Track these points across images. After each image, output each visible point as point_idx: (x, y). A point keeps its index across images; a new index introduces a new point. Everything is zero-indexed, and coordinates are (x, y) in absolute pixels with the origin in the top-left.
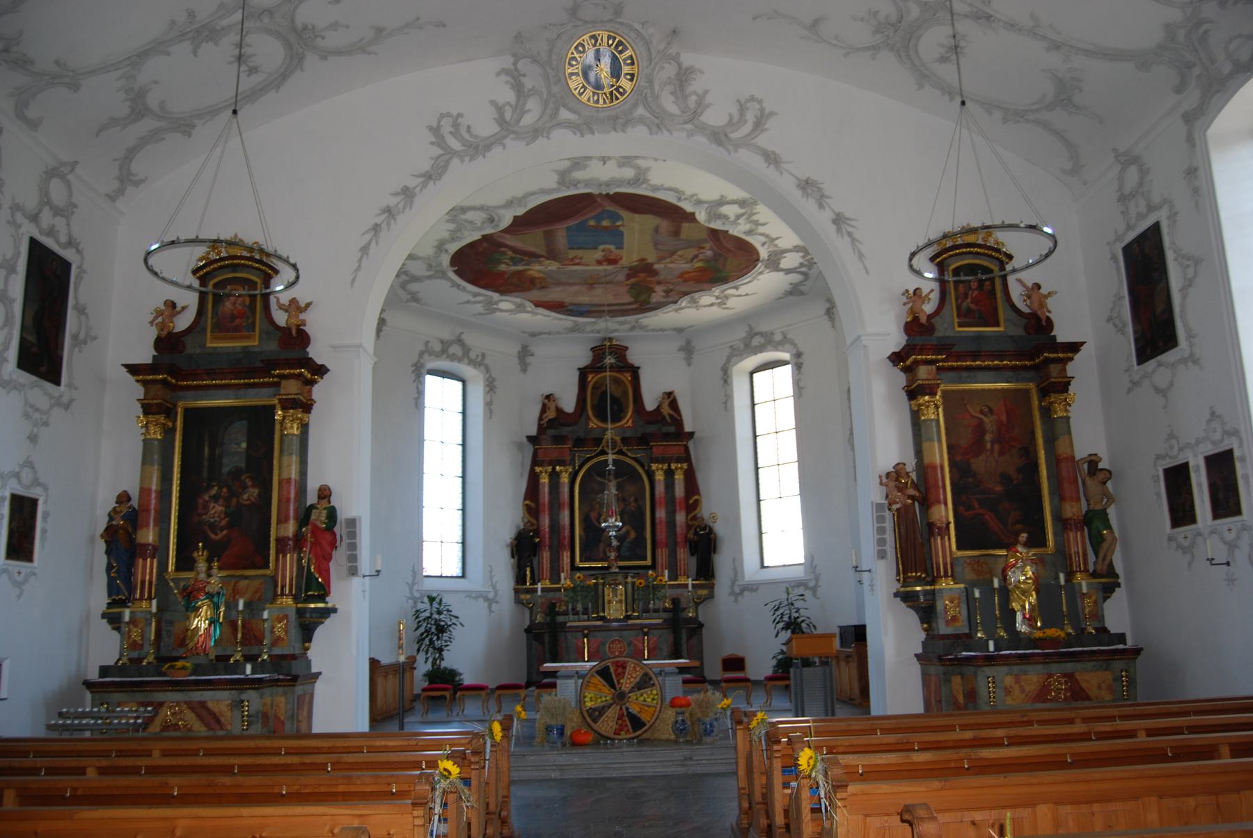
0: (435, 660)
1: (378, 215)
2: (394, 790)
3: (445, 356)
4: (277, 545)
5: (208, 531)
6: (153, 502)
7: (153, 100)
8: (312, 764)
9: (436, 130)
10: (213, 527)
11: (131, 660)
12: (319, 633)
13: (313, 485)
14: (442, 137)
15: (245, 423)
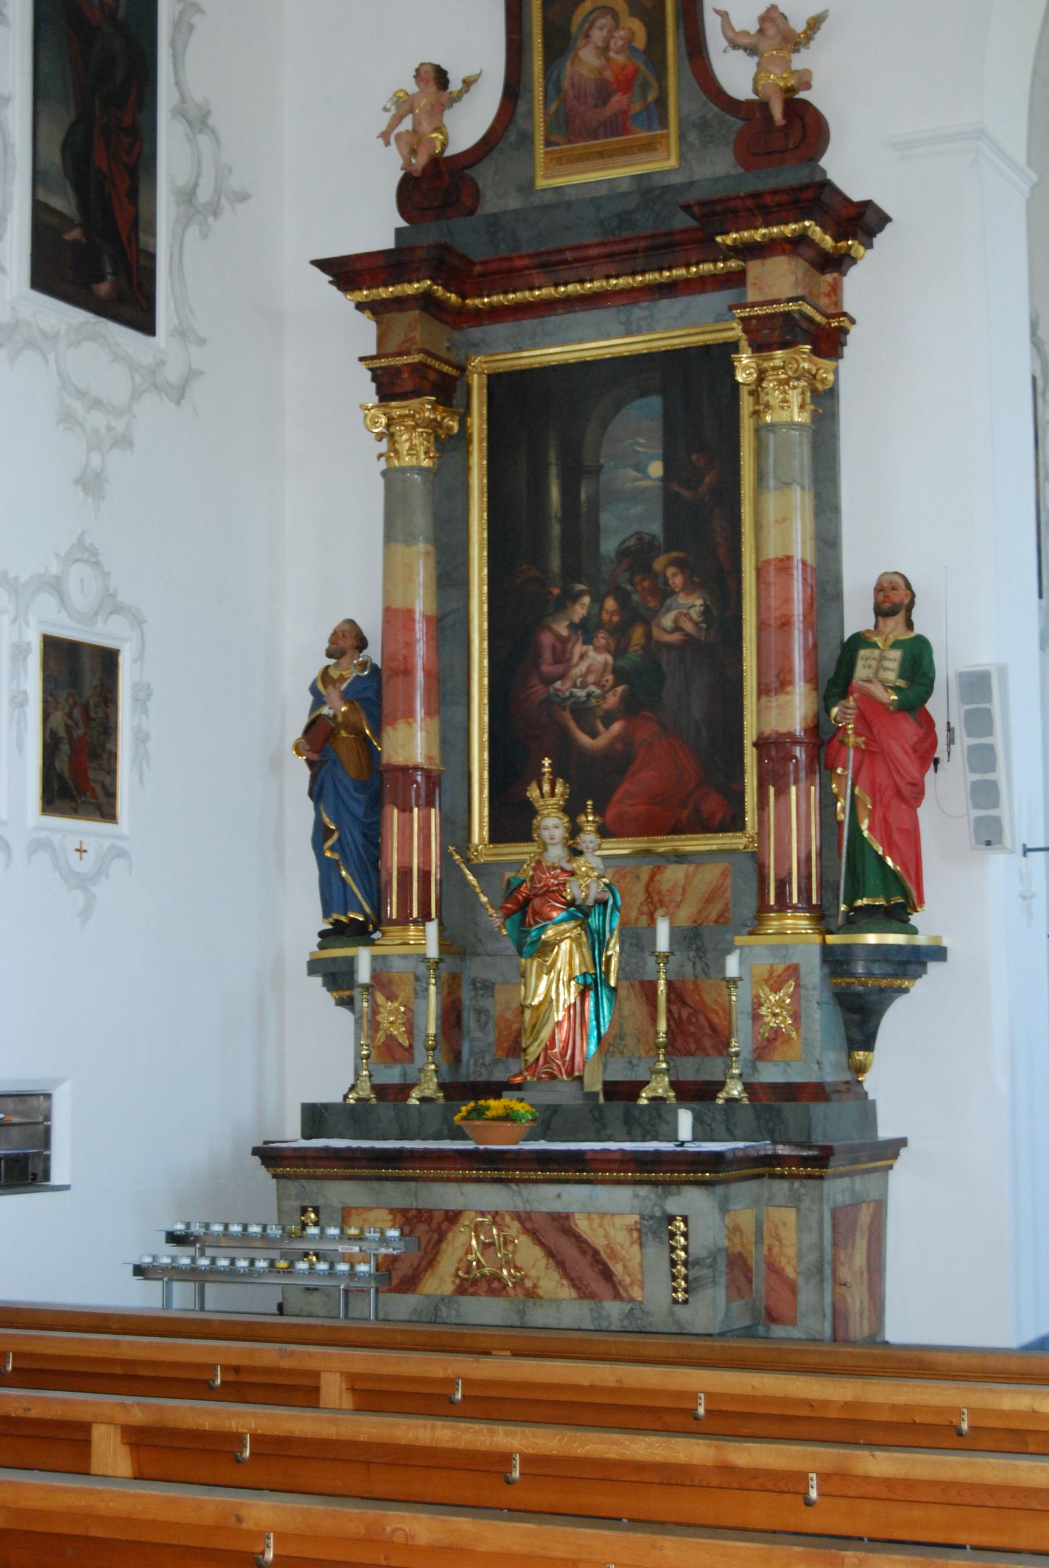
6: (421, 649)
10: (582, 712)
11: (380, 1090)
15: (655, 402)
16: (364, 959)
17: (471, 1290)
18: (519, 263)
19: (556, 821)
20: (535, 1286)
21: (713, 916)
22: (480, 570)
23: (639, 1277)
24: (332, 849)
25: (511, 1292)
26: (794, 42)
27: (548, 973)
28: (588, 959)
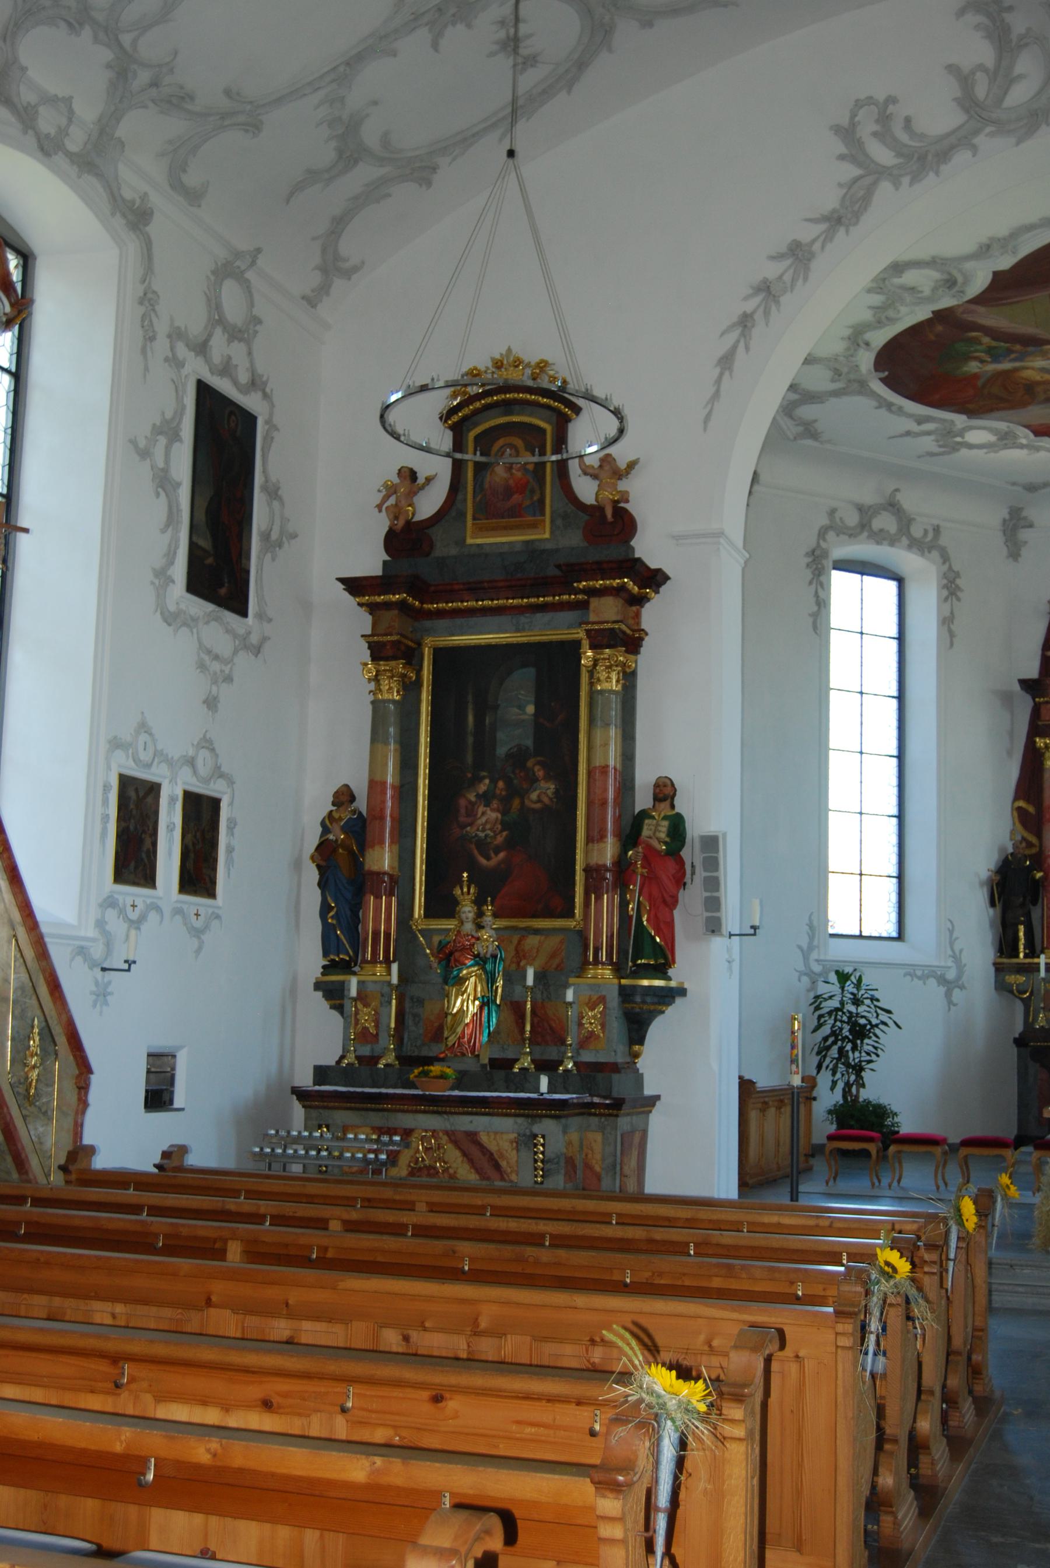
0: (848, 1085)
1: (746, 298)
2: (800, 1293)
3: (865, 534)
4: (587, 879)
5: (476, 852)
6: (389, 804)
7: (370, 135)
8: (664, 1242)
9: (847, 133)
10: (483, 846)
12: (656, 1030)
13: (644, 777)
14: (860, 144)
15: (531, 671)
16: (353, 984)
17: (418, 1174)
18: (456, 587)
19: (470, 909)
20: (455, 1172)
21: (554, 966)
22: (425, 760)
23: (515, 1168)
24: (332, 917)
25: (441, 1176)
26: (620, 474)
27: (462, 995)
28: (486, 988)
